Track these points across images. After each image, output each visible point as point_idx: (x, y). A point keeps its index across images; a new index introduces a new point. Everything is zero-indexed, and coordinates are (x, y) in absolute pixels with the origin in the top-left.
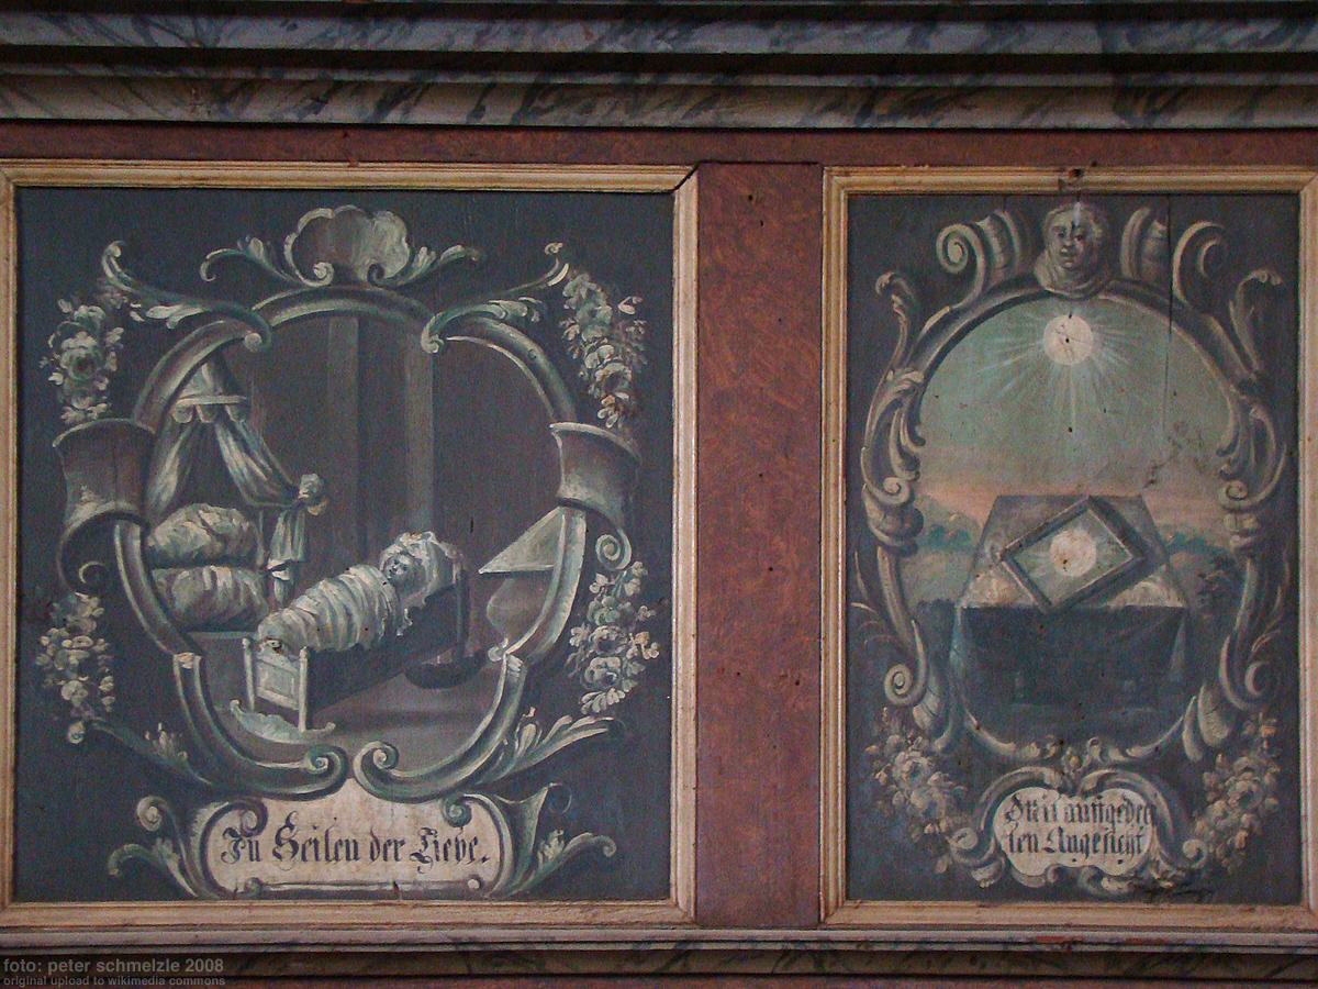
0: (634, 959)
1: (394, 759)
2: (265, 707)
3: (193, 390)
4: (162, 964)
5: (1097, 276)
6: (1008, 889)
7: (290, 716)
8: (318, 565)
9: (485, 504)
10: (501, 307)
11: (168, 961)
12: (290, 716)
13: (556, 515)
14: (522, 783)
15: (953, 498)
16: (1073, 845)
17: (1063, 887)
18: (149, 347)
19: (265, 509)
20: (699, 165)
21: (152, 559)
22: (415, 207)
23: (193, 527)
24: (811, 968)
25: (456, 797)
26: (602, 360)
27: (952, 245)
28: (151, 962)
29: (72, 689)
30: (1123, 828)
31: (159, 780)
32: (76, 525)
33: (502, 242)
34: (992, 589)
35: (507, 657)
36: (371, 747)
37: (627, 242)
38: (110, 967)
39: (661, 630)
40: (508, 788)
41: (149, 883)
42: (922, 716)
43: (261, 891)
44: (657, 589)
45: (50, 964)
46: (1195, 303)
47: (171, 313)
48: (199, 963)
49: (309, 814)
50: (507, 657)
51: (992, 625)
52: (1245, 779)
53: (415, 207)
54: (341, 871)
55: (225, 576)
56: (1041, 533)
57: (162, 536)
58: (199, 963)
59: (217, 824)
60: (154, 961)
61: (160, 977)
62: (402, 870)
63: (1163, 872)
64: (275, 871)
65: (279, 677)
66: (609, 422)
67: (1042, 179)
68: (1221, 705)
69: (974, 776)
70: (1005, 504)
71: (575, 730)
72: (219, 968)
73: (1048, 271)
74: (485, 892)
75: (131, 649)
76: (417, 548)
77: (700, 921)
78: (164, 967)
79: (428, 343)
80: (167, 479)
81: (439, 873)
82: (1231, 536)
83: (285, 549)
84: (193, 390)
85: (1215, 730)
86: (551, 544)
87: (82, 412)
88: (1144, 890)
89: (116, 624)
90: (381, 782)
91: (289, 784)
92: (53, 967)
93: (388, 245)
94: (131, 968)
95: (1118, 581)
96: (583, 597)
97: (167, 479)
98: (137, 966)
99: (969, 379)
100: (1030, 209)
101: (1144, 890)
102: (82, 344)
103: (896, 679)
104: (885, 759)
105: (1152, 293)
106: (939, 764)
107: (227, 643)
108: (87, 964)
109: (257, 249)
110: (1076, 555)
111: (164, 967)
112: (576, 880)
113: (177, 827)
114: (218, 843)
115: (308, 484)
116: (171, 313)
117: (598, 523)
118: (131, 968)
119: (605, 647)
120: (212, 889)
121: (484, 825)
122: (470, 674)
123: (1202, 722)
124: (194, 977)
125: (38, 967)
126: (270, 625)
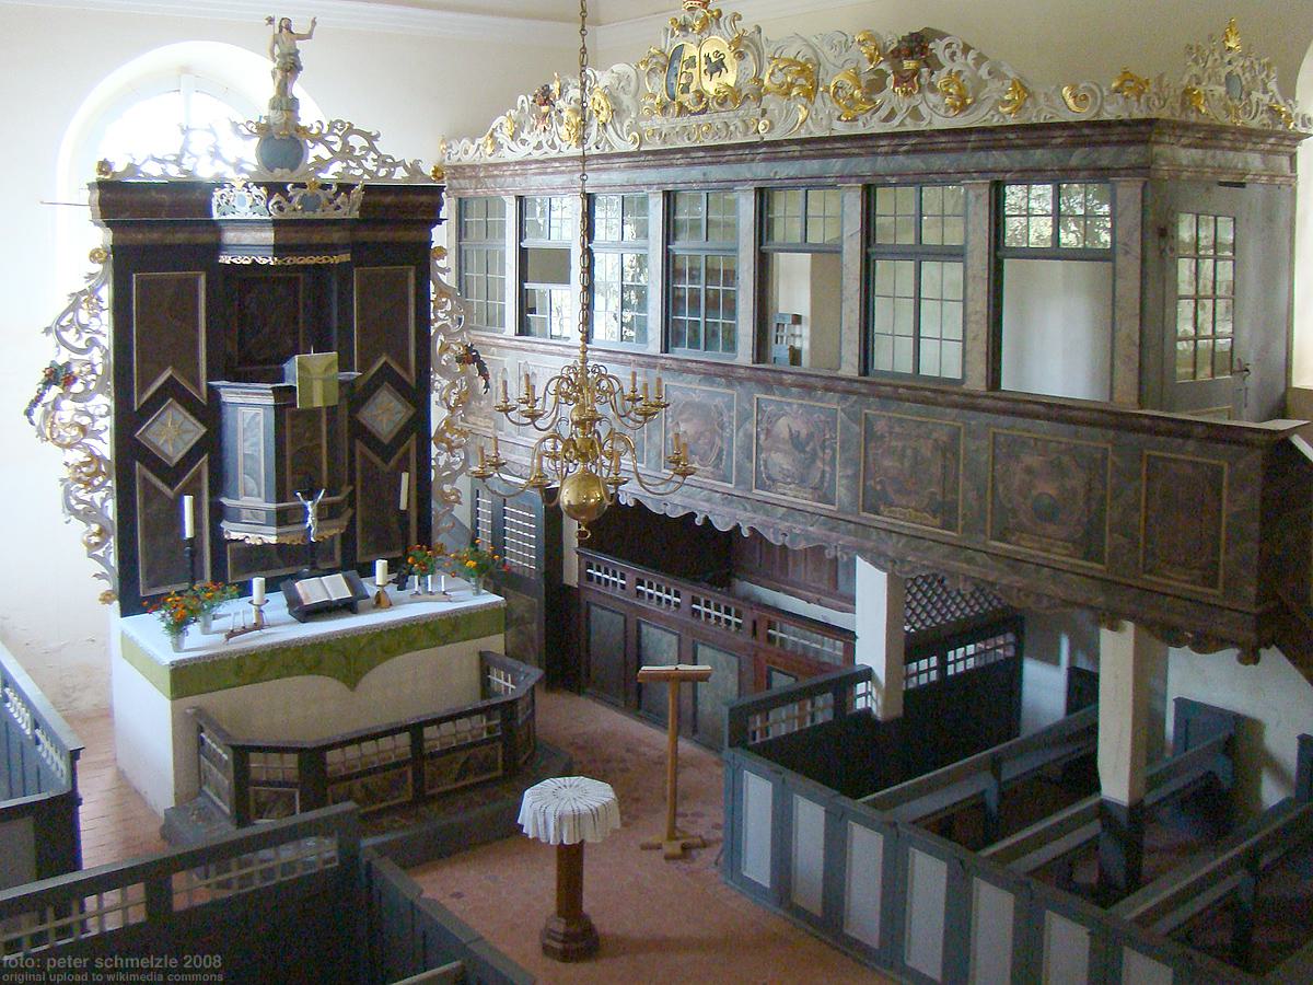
4: (161, 960)
11: (166, 956)
24: (785, 377)
28: (149, 958)
32: (1171, 739)
38: (109, 963)
45: (49, 960)
48: (198, 959)
58: (198, 959)
60: (152, 957)
78: (163, 963)
94: (135, 965)
98: (130, 962)
107: (352, 364)
111: (163, 963)
118: (135, 965)
124: (193, 971)
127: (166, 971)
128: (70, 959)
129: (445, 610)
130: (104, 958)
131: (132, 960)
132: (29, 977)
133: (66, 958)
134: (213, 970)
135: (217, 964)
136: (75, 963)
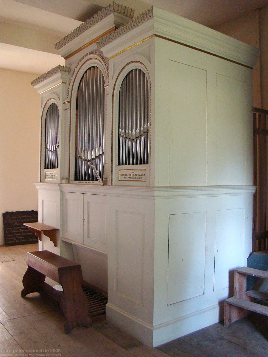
45: (14, 350)
94: (36, 351)
111: (44, 351)
118: (36, 351)
125: (10, 351)
131: (36, 350)
135: (59, 351)
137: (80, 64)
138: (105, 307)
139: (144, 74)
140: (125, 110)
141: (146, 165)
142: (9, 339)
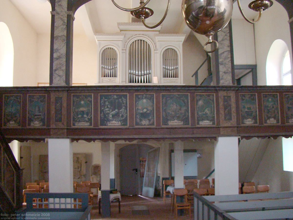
0: (126, 129)
1: (116, 119)
2: (110, 117)
3: (107, 103)
5: (146, 98)
6: (142, 125)
7: (111, 118)
8: (112, 111)
9: (120, 108)
10: (120, 99)
12: (111, 118)
13: (123, 109)
14: (121, 121)
15: (140, 108)
16: (145, 123)
17: (144, 125)
18: (105, 101)
19: (110, 108)
20: (128, 93)
21: (105, 111)
22: (116, 95)
23: (107, 109)
25: (118, 121)
26: (124, 102)
27: (139, 96)
29: (102, 117)
30: (147, 122)
31: (106, 120)
33: (120, 97)
34: (141, 112)
35: (121, 115)
36: (115, 119)
37: (125, 96)
39: (127, 114)
40: (120, 121)
41: (105, 125)
42: (138, 117)
43: (110, 126)
44: (127, 112)
45: (11, 214)
46: (150, 99)
47: (106, 100)
48: (47, 214)
49: (112, 122)
50: (121, 115)
51: (141, 113)
52: (152, 120)
53: (116, 95)
54: (114, 125)
55: (108, 112)
56: (144, 109)
57: (106, 110)
58: (47, 214)
59: (108, 123)
61: (36, 217)
62: (116, 125)
63: (149, 124)
64: (110, 125)
65: (111, 116)
66: (125, 104)
67: (143, 94)
68: (151, 117)
69: (141, 120)
70: (142, 108)
71: (123, 118)
72: (49, 215)
73: (144, 98)
74: (119, 126)
75: (104, 115)
76: (117, 110)
77: (129, 127)
78: (36, 215)
79: (117, 101)
80: (106, 107)
81: (118, 125)
82: (152, 109)
83: (111, 111)
84: (107, 103)
85: (151, 118)
86: (122, 110)
87: (102, 104)
88: (148, 125)
89: (104, 114)
90: (115, 121)
91: (111, 121)
92: (12, 215)
93: (115, 97)
94: (29, 215)
95: (146, 112)
96: (124, 113)
97: (106, 107)
99: (140, 102)
100: (143, 95)
101: (148, 125)
102: (102, 101)
103: (137, 116)
104: (137, 119)
105: (148, 99)
106: (139, 120)
108: (19, 214)
109: (110, 97)
110: (145, 110)
111: (36, 215)
112: (124, 125)
113: (106, 123)
114: (108, 123)
115: (112, 107)
116: (106, 100)
117: (124, 109)
118: (29, 215)
119: (125, 114)
120: (108, 125)
121: (120, 123)
122: (119, 116)
123: (150, 118)
125: (8, 215)
126: (110, 114)
127: (37, 217)
128: (5, 214)
129: (16, 159)
130: (23, 214)
131: (30, 214)
132: (7, 218)
133: (15, 214)
134: (48, 217)
135: (49, 215)
136: (32, 215)
137: (137, 36)
138: (74, 170)
139: (176, 52)
140: (146, 56)
141: (115, 78)
142: (9, 201)
